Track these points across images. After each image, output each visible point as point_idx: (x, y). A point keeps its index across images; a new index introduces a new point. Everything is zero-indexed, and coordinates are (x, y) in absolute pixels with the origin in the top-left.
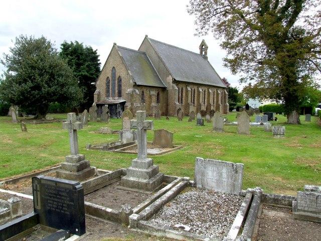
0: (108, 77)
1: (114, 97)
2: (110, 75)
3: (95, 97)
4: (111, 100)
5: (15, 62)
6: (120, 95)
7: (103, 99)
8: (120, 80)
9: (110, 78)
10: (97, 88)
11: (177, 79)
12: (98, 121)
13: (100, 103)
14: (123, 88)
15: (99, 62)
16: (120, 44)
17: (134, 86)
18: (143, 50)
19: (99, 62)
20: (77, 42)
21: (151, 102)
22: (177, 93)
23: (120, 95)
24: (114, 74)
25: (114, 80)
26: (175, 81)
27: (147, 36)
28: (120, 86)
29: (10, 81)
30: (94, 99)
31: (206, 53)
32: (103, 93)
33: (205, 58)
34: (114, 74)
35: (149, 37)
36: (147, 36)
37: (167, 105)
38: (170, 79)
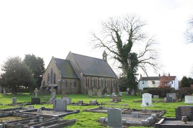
0: (49, 74)
1: (51, 84)
2: (50, 72)
3: (42, 83)
4: (50, 85)
5: (5, 67)
6: (55, 83)
7: (46, 84)
8: (55, 76)
9: (50, 74)
10: (43, 79)
11: (85, 74)
12: (179, 101)
13: (44, 87)
14: (56, 79)
15: (44, 64)
16: (56, 57)
17: (62, 78)
18: (68, 59)
19: (44, 64)
20: (45, 64)
21: (71, 87)
22: (85, 81)
23: (55, 83)
24: (52, 72)
25: (52, 75)
26: (84, 75)
27: (70, 52)
28: (55, 78)
29: (3, 76)
30: (179, 124)
31: (106, 58)
32: (46, 81)
33: (106, 61)
34: (52, 72)
35: (71, 52)
36: (70, 52)
37: (73, 78)
38: (82, 74)
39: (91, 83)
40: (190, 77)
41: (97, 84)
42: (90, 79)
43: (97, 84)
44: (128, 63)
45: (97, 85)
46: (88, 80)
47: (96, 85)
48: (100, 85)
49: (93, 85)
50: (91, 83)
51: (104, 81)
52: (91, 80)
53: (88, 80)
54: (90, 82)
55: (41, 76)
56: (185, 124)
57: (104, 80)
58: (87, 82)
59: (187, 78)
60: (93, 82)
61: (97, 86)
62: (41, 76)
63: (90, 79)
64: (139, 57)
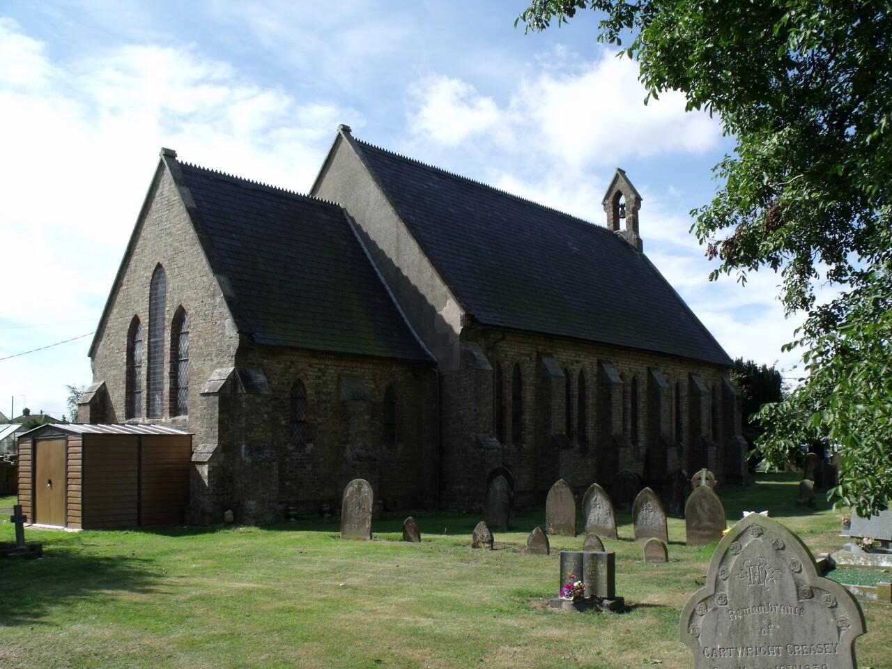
39: (543, 400)
40: (369, 233)
41: (591, 411)
42: (529, 369)
43: (591, 411)
44: (720, 532)
45: (591, 423)
46: (508, 376)
47: (582, 424)
48: (617, 424)
49: (558, 424)
50: (543, 400)
51: (529, 379)
52: (544, 379)
53: (508, 376)
54: (529, 396)
55: (753, 13)
56: (680, 451)
57: (643, 378)
58: (499, 396)
59: (732, 361)
60: (558, 404)
61: (591, 434)
62: (753, 13)
63: (529, 369)
64: (621, 572)
